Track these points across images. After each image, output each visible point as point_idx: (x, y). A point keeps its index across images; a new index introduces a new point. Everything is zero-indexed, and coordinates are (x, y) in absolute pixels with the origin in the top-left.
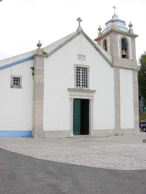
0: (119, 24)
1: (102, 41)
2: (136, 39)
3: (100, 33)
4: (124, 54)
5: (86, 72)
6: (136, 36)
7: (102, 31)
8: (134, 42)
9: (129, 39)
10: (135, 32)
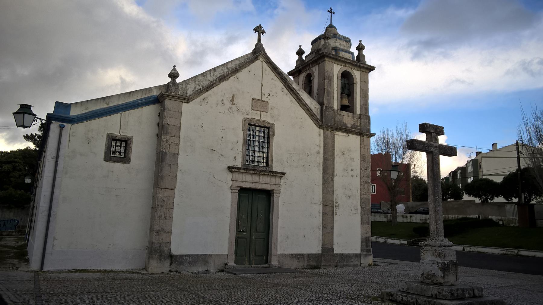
0: (338, 44)
1: (302, 76)
2: (371, 74)
3: (300, 61)
4: (346, 102)
5: (266, 135)
6: (372, 69)
7: (304, 57)
8: (365, 82)
9: (357, 74)
10: (370, 61)
